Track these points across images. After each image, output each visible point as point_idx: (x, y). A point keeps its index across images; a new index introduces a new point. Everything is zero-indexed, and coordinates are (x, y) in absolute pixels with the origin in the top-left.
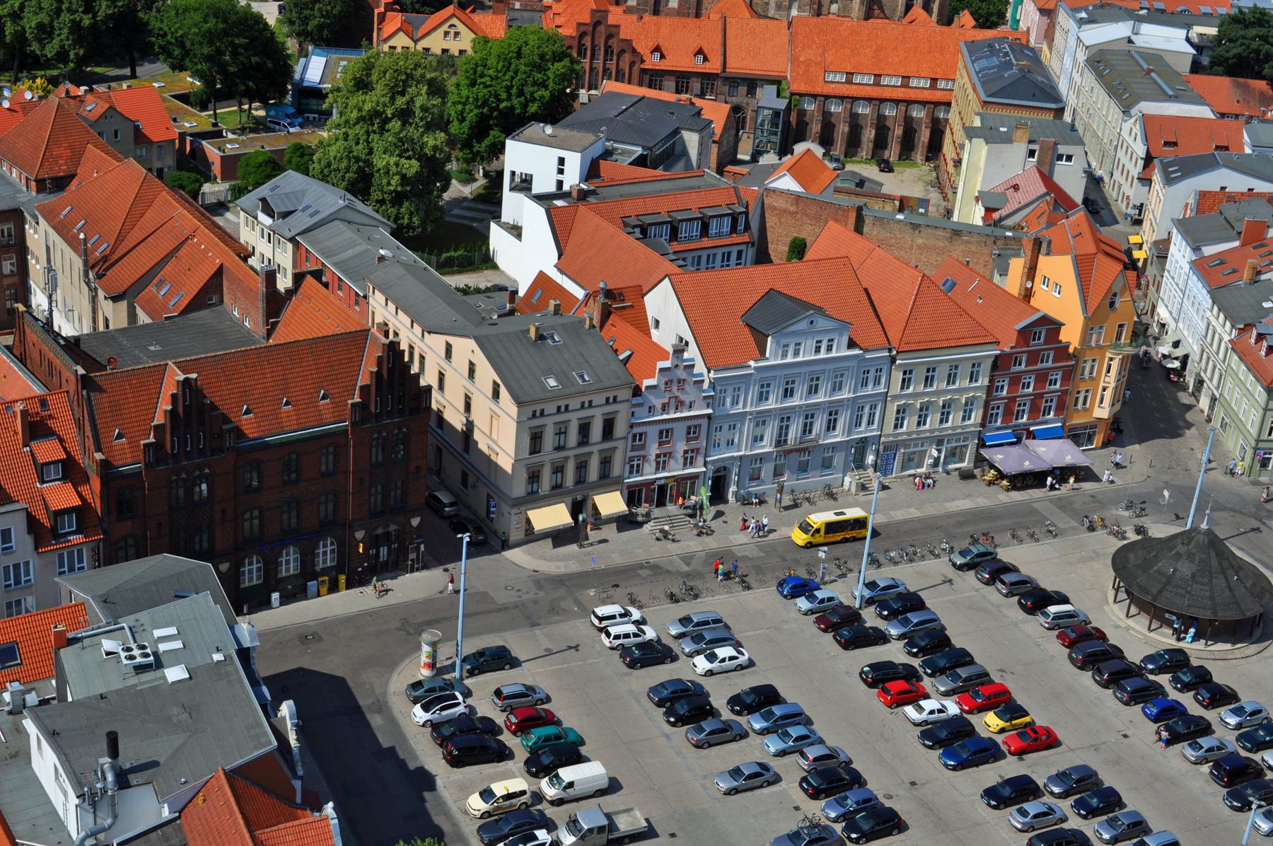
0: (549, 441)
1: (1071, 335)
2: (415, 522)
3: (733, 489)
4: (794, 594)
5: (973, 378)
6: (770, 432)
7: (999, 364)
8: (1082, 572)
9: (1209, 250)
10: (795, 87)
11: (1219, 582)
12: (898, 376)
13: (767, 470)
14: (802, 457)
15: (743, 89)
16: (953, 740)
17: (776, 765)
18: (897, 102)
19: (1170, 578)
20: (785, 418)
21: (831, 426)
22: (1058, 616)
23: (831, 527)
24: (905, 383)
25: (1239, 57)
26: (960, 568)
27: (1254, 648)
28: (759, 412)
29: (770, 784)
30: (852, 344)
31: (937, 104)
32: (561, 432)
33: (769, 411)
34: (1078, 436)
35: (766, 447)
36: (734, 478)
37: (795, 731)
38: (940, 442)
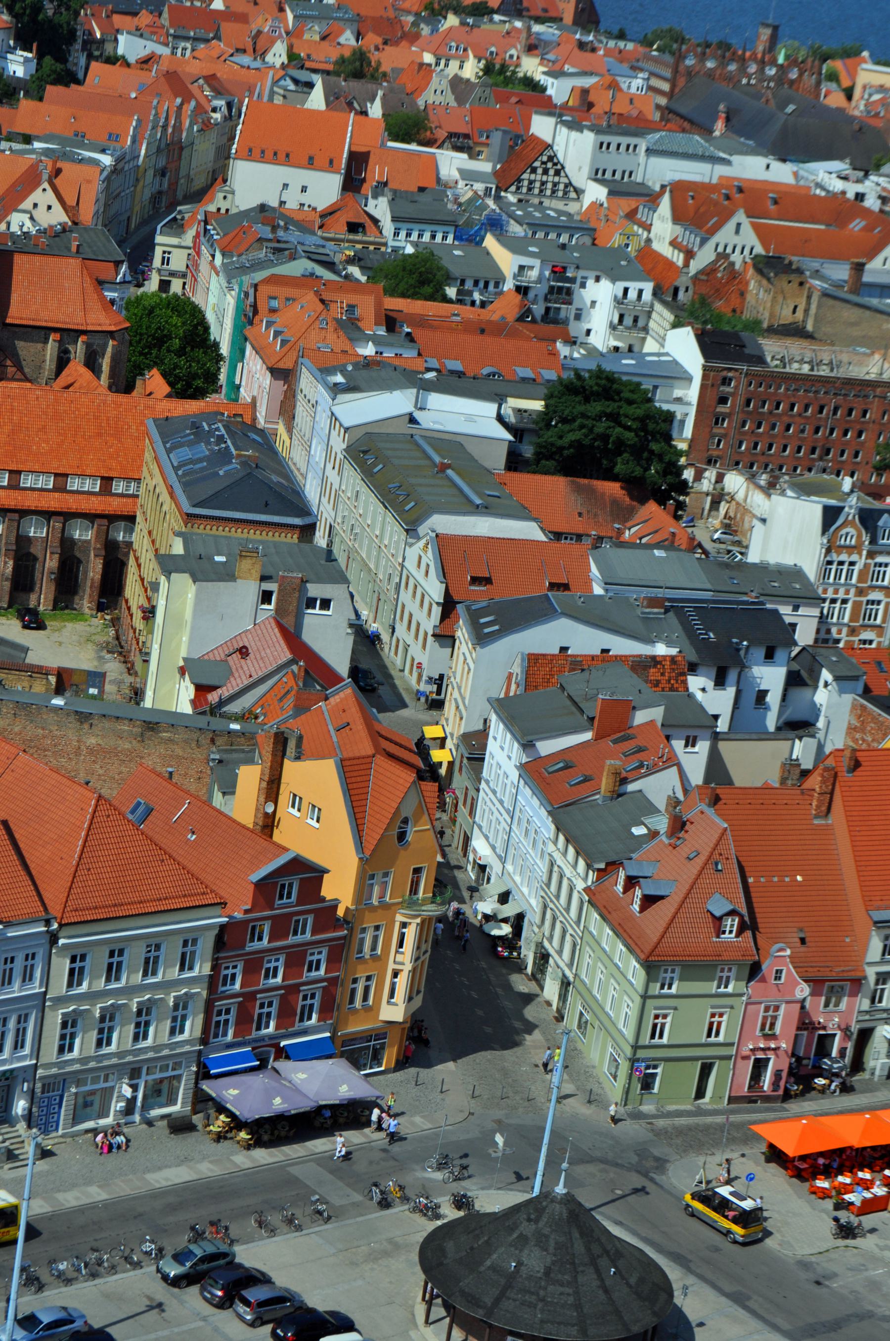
1: (339, 889)
5: (185, 963)
7: (226, 939)
9: (547, 747)
11: (588, 1279)
12: (62, 966)
18: (48, 515)
25: (577, 445)
26: (176, 1282)
31: (112, 518)
34: (359, 1052)
38: (134, 1073)
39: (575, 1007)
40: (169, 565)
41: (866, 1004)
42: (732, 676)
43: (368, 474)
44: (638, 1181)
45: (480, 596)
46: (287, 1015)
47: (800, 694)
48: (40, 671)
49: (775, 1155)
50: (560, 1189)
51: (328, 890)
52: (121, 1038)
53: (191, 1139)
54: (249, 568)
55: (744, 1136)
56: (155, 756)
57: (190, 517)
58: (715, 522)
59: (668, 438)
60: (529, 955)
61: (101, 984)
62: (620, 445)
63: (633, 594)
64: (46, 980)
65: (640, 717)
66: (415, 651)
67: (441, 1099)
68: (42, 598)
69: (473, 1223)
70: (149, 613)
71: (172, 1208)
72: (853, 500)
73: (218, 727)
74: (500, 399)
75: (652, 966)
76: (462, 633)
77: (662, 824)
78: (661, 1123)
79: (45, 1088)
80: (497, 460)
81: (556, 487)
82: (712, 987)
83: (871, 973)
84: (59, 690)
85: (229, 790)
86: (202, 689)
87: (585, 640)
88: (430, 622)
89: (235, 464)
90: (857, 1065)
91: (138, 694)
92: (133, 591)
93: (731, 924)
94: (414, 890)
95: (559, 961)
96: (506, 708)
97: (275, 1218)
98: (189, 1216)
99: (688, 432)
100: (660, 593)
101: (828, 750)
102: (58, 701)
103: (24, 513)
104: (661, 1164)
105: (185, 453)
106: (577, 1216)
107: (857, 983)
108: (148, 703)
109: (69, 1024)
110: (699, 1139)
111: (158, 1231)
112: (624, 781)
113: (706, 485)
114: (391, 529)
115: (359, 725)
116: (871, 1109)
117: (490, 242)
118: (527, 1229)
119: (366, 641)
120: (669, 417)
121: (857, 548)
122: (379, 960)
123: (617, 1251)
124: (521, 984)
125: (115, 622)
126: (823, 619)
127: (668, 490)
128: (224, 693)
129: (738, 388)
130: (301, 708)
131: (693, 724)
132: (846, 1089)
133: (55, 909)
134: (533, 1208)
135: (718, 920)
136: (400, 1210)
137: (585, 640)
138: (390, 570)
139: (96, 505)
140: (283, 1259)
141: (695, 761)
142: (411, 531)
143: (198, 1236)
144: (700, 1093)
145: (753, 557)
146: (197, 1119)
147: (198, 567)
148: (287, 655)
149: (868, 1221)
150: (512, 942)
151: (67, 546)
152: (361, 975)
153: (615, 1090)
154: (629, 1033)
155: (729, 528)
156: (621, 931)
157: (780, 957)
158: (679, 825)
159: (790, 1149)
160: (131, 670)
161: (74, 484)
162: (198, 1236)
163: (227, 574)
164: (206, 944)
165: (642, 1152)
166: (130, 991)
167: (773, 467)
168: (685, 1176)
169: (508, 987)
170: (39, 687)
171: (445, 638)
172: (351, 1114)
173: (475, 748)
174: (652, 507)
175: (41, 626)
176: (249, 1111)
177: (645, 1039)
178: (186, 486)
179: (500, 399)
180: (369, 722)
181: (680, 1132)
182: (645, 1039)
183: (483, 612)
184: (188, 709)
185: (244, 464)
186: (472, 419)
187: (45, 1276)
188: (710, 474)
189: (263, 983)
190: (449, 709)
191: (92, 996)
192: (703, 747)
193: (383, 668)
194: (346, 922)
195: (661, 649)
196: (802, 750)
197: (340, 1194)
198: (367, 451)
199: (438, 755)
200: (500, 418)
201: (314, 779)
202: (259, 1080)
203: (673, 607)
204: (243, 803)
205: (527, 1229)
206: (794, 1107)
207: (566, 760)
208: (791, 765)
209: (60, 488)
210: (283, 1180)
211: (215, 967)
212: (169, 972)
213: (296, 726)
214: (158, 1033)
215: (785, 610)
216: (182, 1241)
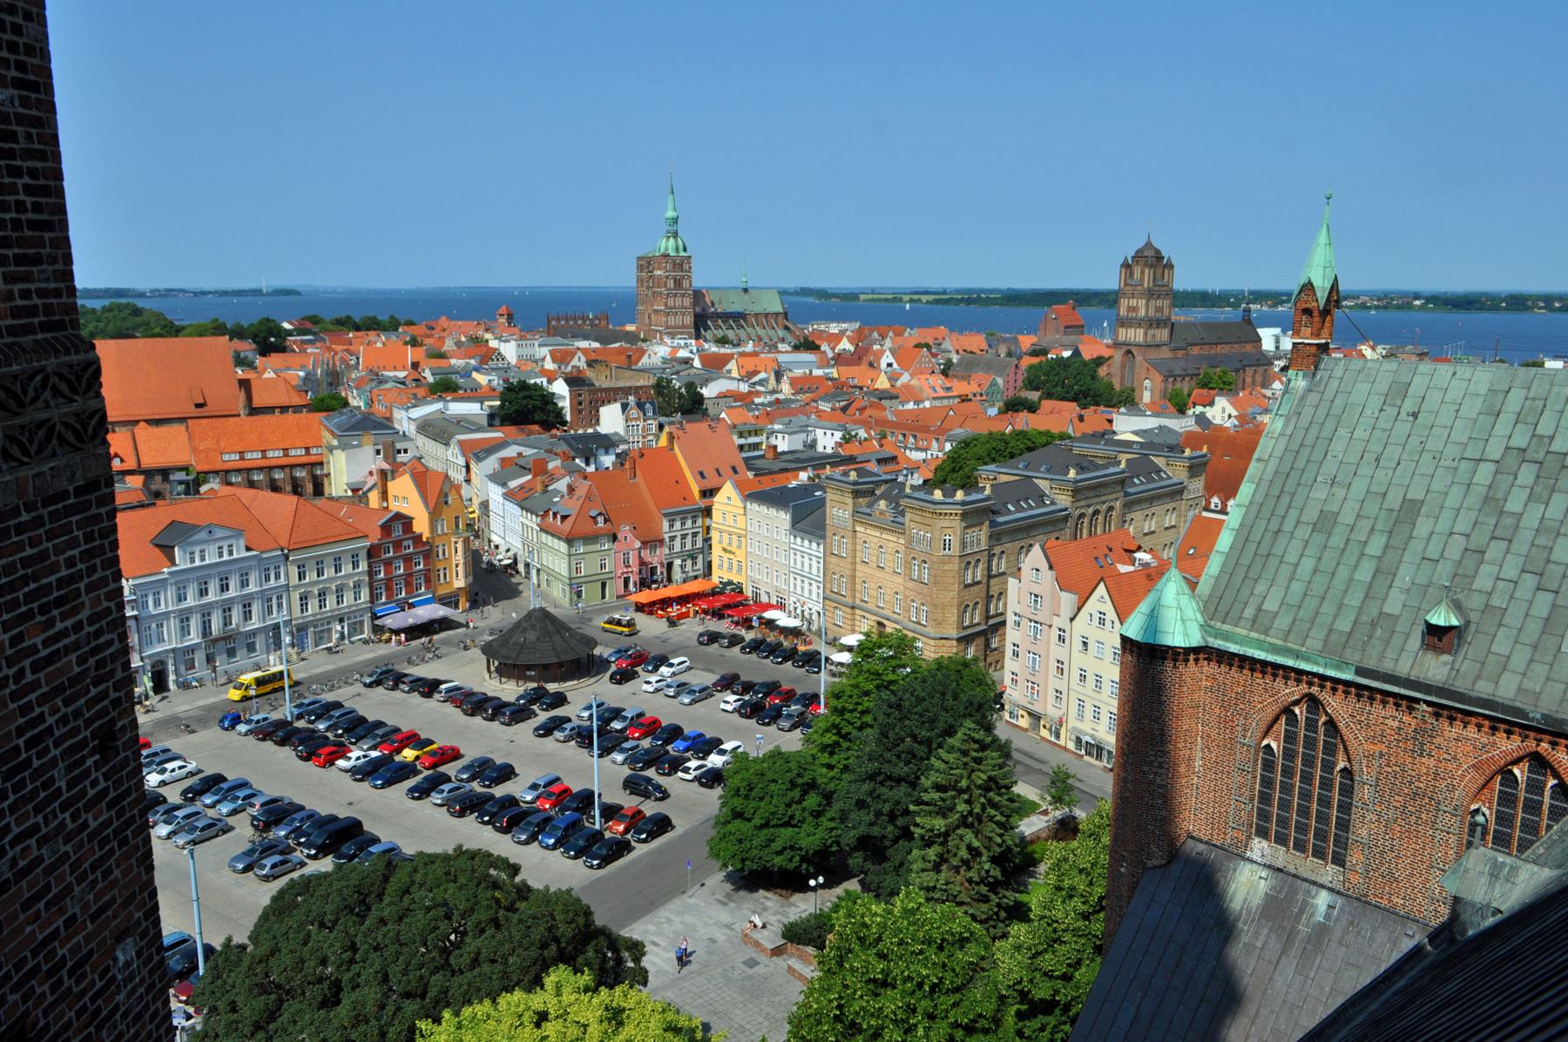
1: (421, 526)
3: (172, 677)
4: (233, 727)
5: (355, 565)
6: (195, 624)
7: (372, 553)
8: (469, 670)
9: (513, 484)
10: (199, 468)
11: (557, 639)
12: (294, 571)
13: (200, 658)
14: (229, 643)
15: (158, 478)
16: (382, 772)
17: (231, 821)
18: (282, 467)
19: (522, 646)
20: (206, 612)
21: (247, 615)
22: (448, 691)
23: (260, 682)
24: (301, 576)
25: (517, 411)
26: (369, 686)
27: (593, 680)
28: (181, 611)
29: (225, 832)
30: (248, 549)
31: (313, 465)
33: (190, 608)
34: (450, 601)
35: (194, 638)
36: (171, 668)
37: (241, 793)
38: (341, 621)
65: (551, 466)
79: (299, 630)
82: (598, 547)
83: (666, 537)
93: (601, 519)
107: (661, 541)
109: (304, 598)
114: (441, 448)
117: (475, 375)
122: (450, 559)
129: (585, 397)
135: (594, 518)
144: (603, 597)
154: (566, 574)
157: (625, 531)
161: (293, 453)
172: (444, 624)
198: (425, 427)
209: (286, 455)
211: (370, 566)
212: (347, 569)
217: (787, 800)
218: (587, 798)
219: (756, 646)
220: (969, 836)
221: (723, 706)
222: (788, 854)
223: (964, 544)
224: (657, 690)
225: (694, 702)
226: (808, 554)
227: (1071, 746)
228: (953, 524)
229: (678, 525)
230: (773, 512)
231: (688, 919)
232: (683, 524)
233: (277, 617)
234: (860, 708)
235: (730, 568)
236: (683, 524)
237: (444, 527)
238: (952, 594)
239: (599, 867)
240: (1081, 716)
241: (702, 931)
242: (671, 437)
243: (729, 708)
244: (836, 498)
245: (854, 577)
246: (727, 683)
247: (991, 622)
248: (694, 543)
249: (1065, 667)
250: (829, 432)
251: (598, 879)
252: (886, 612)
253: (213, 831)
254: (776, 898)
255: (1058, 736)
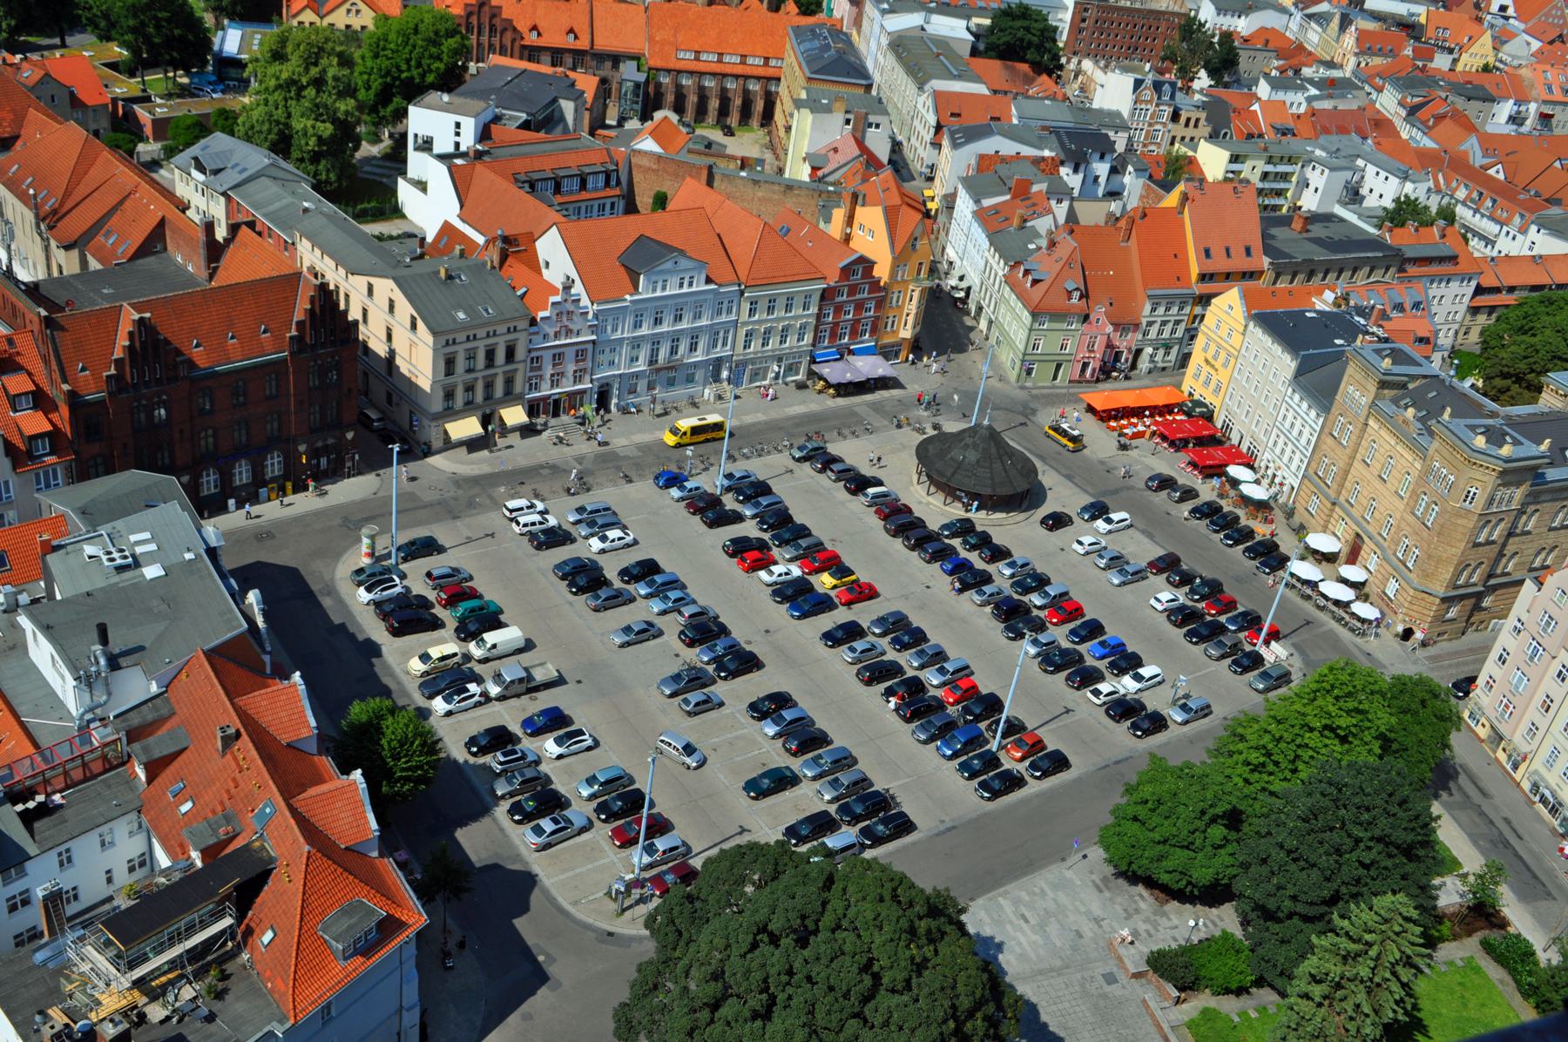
0: (461, 365)
1: (882, 272)
2: (350, 435)
3: (614, 401)
6: (644, 355)
7: (825, 295)
9: (987, 202)
11: (997, 465)
12: (746, 307)
13: (642, 385)
14: (669, 374)
15: (608, 64)
16: (798, 597)
18: (737, 77)
20: (656, 341)
21: (693, 348)
22: (876, 496)
23: (695, 431)
24: (752, 312)
25: (1007, 44)
26: (798, 460)
27: (1023, 516)
30: (709, 281)
31: (769, 79)
32: (471, 357)
34: (888, 353)
35: (641, 366)
36: (616, 392)
37: (673, 595)
38: (780, 360)
39: (995, 334)
40: (799, 104)
41: (1140, 337)
42: (1082, 168)
43: (899, 57)
44: (1023, 420)
45: (955, 124)
46: (854, 333)
47: (1116, 178)
48: (733, 158)
49: (1090, 409)
50: (986, 422)
51: (876, 273)
52: (773, 343)
53: (805, 392)
54: (840, 107)
55: (1075, 399)
56: (791, 202)
57: (810, 79)
58: (1076, 86)
59: (1055, 41)
60: (973, 308)
61: (765, 316)
62: (1030, 44)
63: (1033, 123)
64: (738, 314)
65: (1035, 188)
66: (920, 151)
67: (926, 376)
68: (733, 120)
69: (942, 438)
70: (788, 129)
71: (797, 425)
72: (1150, 76)
73: (823, 188)
74: (968, 18)
75: (1035, 315)
76: (946, 142)
77: (1044, 243)
78: (1035, 392)
80: (965, 51)
81: (995, 66)
82: (1065, 326)
83: (1144, 321)
84: (742, 168)
85: (828, 220)
86: (814, 169)
87: (1007, 147)
88: (928, 136)
89: (833, 52)
90: (1134, 366)
91: (781, 171)
92: (778, 116)
93: (1076, 294)
94: (919, 273)
95: (988, 311)
96: (967, 182)
97: (846, 432)
98: (805, 429)
99: (1064, 38)
100: (1048, 123)
101: (1129, 208)
102: (743, 174)
103: (724, 75)
104: (1034, 412)
105: (807, 45)
106: (993, 436)
107: (1137, 326)
108: (787, 175)
109: (749, 334)
110: (1052, 400)
111: (791, 436)
112: (1025, 221)
113: (1072, 66)
115: (894, 189)
116: (1140, 388)
118: (968, 440)
119: (896, 146)
120: (1056, 28)
121: (1150, 102)
122: (900, 308)
123: (1011, 453)
124: (969, 322)
125: (769, 133)
126: (1130, 139)
127: (1048, 65)
128: (826, 171)
130: (865, 179)
131: (1060, 192)
132: (1127, 378)
133: (743, 279)
134: (972, 431)
135: (1069, 293)
136: (906, 430)
137: (1007, 147)
138: (911, 109)
139: (761, 72)
140: (852, 452)
141: (1061, 211)
142: (921, 88)
143: (809, 439)
144: (1055, 378)
145: (1095, 105)
146: (809, 383)
147: (813, 105)
148: (857, 152)
149: (1135, 442)
150: (964, 301)
151: (746, 94)
152: (891, 315)
153: (1013, 375)
154: (1021, 347)
155: (1082, 89)
156: (1020, 296)
157: (1099, 312)
158: (1052, 244)
159: (1098, 407)
160: (777, 158)
162: (809, 439)
163: (828, 110)
164: (816, 298)
165: (1025, 406)
166: (778, 320)
167: (1108, 56)
168: (1046, 418)
169: (962, 323)
170: (732, 166)
171: (937, 145)
173: (950, 202)
174: (1044, 77)
175: (732, 135)
176: (833, 380)
177: (1030, 350)
178: (808, 63)
179: (968, 18)
180: (899, 188)
181: (1043, 396)
182: (1030, 350)
183: (957, 131)
184: (807, 179)
185: (838, 51)
186: (953, 29)
187: (736, 455)
188: (1075, 60)
189: (843, 318)
190: (937, 181)
191: (760, 322)
192: (1066, 204)
193: (904, 160)
194: (884, 288)
195: (1047, 153)
196: (1114, 206)
197: (877, 421)
198: (900, 45)
199: (930, 205)
200: (968, 29)
201: (871, 217)
202: (839, 365)
203: (1054, 131)
204: (835, 228)
205: (968, 440)
206: (1101, 386)
207: (997, 209)
208: (1110, 215)
210: (850, 413)
211: (820, 309)
213: (863, 189)
214: (791, 341)
215: (1111, 134)
216: (801, 441)
217: (1191, 828)
218: (993, 705)
219: (1209, 512)
220: (1361, 997)
221: (1153, 602)
222: (1177, 876)
223: (1491, 501)
224: (1088, 553)
225: (1124, 584)
226: (1304, 418)
227: (1526, 786)
228: (1485, 479)
229: (1161, 310)
230: (1277, 349)
231: (1062, 898)
232: (1168, 309)
233: (719, 352)
234: (1299, 741)
235: (1207, 383)
236: (1168, 309)
237: (906, 273)
238: (1455, 550)
239: (989, 799)
240: (1550, 764)
241: (1072, 918)
242: (1185, 198)
243: (1159, 607)
244: (1358, 376)
245: (1347, 472)
246: (1167, 565)
247: (1492, 582)
248: (1173, 331)
249: (1554, 707)
250: (1383, 174)
251: (986, 815)
252: (1370, 529)
253: (645, 636)
254: (1151, 900)
255: (1516, 767)
